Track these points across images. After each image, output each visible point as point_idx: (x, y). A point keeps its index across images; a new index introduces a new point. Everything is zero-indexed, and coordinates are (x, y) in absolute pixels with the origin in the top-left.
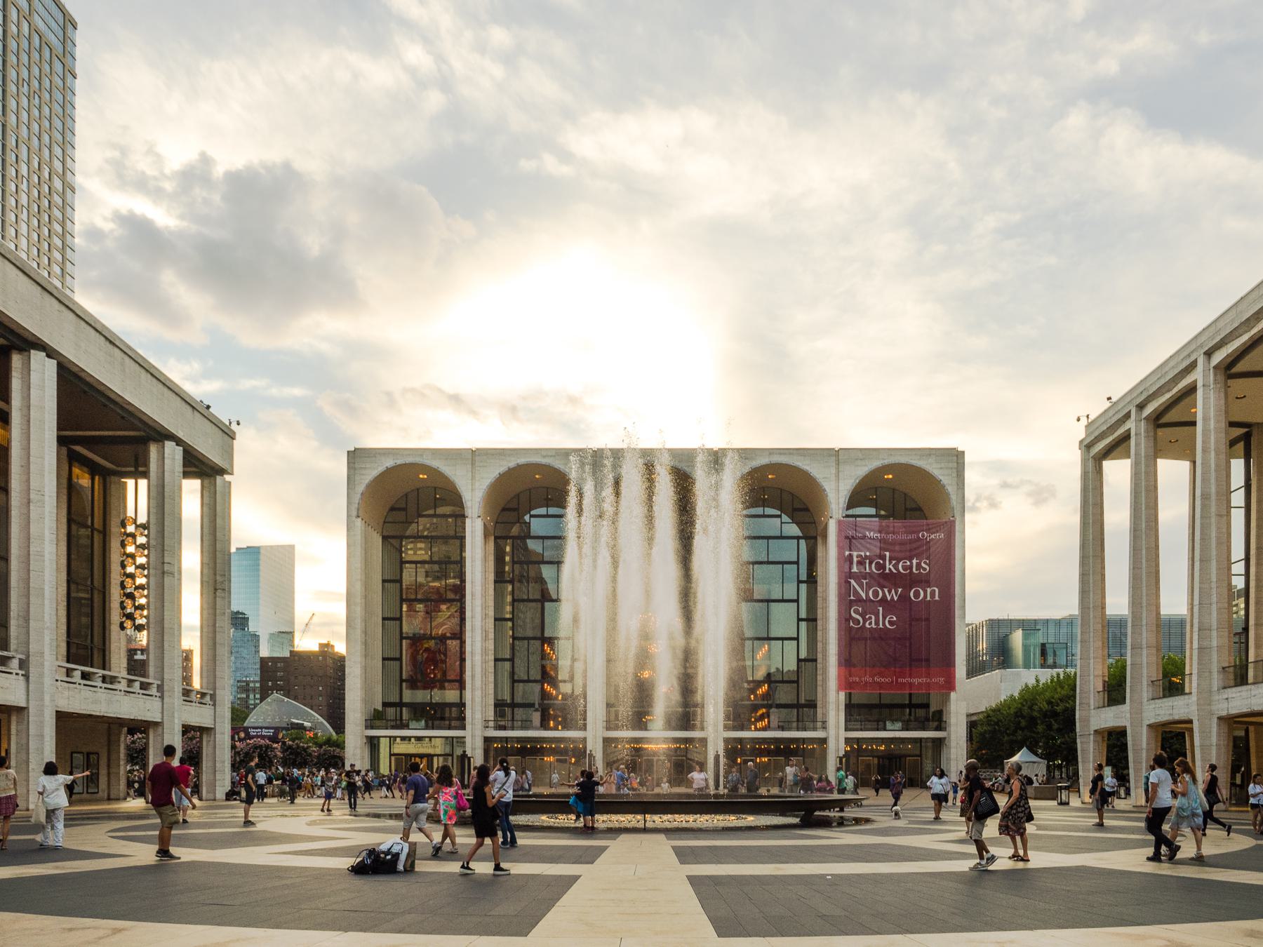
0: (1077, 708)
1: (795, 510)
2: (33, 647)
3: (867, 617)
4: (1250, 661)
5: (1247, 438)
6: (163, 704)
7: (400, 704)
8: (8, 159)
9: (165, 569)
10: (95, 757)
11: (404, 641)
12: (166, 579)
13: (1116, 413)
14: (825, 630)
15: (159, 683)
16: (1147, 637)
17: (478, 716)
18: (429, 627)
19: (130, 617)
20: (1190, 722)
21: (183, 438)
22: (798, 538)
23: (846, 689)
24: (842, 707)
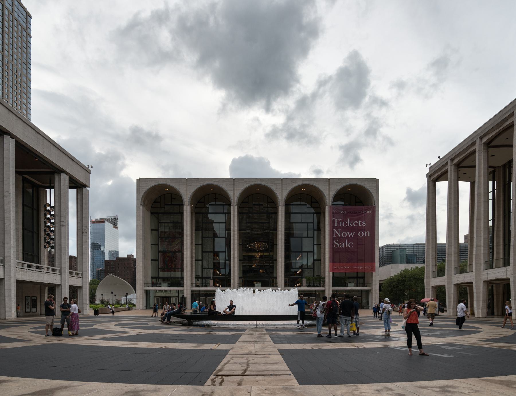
0: (425, 278)
1: (312, 202)
2: (6, 254)
3: (341, 243)
4: (494, 259)
5: (494, 172)
6: (83, 280)
7: (158, 278)
8: (4, 68)
9: (62, 224)
10: (33, 297)
11: (159, 253)
12: (62, 228)
13: (442, 163)
14: (324, 248)
15: (60, 269)
16: (453, 250)
17: (189, 282)
18: (169, 248)
19: (48, 243)
20: (472, 283)
21: (68, 172)
22: (314, 213)
23: (332, 271)
24: (331, 278)
